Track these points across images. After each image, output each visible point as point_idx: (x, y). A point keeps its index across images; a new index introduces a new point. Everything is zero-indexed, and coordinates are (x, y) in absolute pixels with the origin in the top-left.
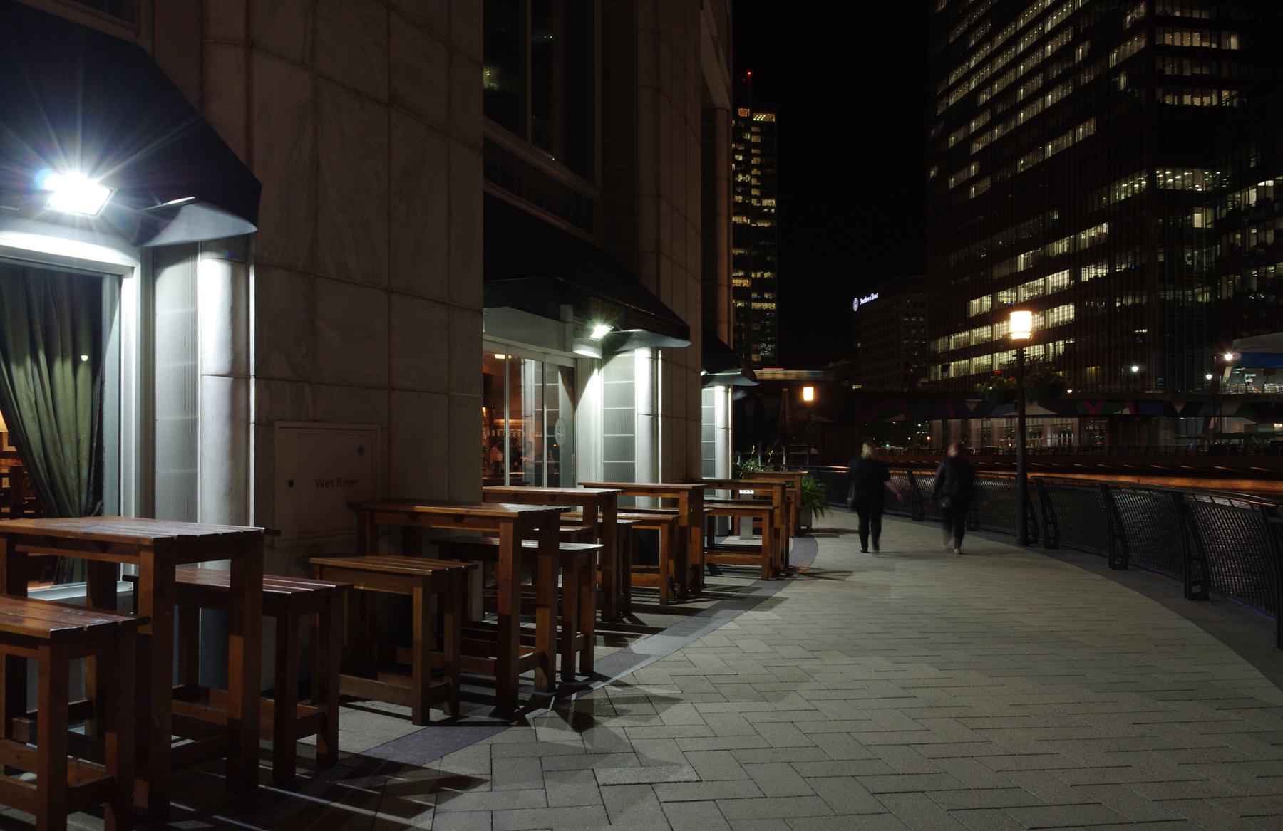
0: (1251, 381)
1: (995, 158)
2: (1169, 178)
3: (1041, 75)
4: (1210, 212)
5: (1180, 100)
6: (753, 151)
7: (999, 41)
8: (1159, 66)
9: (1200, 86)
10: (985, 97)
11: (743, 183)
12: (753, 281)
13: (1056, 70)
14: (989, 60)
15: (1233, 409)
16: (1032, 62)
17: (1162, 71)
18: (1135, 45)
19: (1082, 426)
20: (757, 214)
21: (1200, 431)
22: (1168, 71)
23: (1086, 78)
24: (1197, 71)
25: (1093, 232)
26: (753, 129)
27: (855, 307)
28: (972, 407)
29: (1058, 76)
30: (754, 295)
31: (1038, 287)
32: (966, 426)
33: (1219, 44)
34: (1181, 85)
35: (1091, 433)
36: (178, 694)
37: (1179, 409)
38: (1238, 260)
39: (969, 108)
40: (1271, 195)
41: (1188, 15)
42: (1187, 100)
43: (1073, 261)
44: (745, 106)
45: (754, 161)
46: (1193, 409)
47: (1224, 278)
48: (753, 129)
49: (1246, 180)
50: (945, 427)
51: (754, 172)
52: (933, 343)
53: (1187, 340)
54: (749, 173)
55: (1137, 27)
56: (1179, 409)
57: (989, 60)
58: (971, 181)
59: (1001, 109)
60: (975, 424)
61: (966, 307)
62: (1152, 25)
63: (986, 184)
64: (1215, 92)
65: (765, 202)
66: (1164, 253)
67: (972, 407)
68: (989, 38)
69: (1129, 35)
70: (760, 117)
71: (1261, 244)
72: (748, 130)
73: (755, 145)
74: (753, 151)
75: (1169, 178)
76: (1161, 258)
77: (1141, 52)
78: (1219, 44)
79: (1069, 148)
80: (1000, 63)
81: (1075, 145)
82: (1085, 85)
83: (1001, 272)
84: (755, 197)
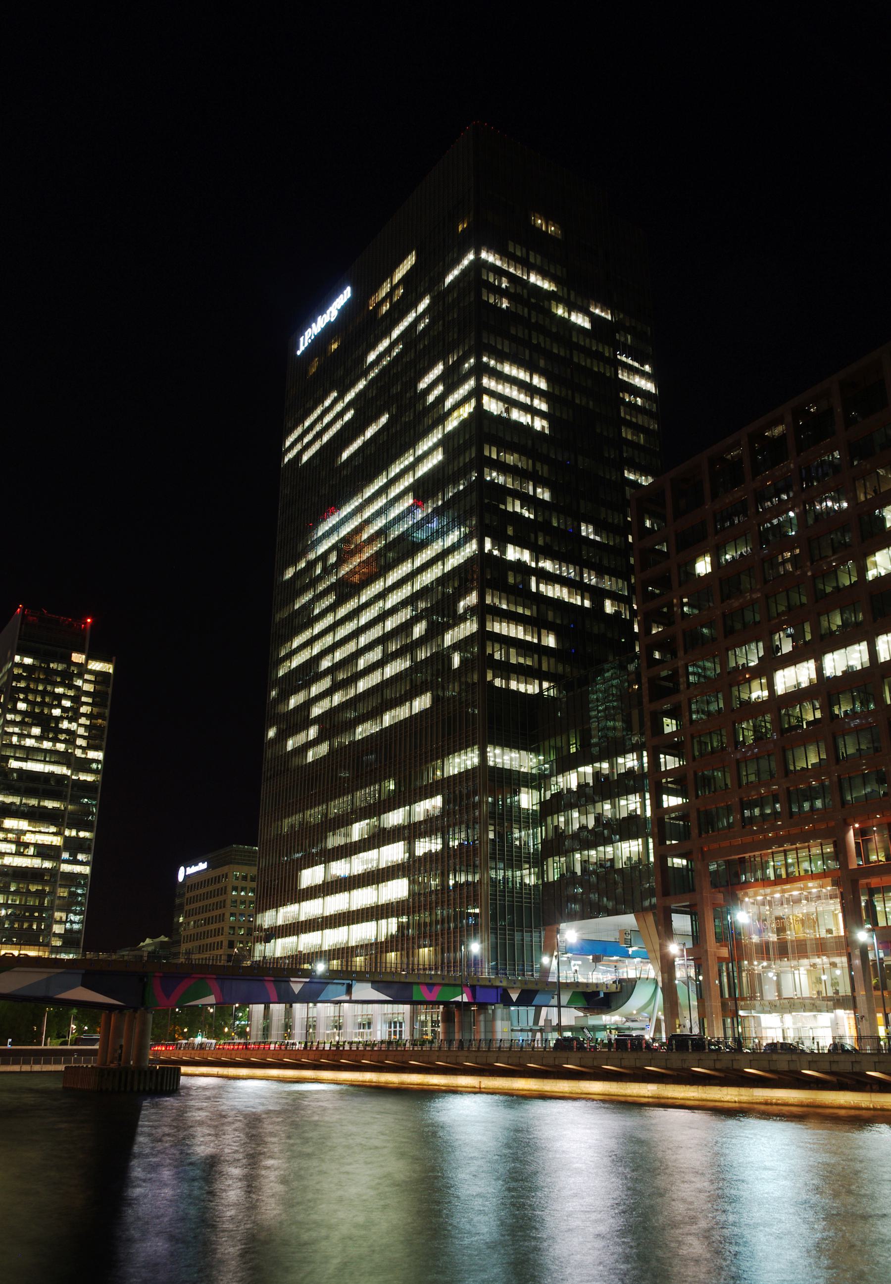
0: (577, 968)
1: (331, 724)
2: (502, 757)
3: (380, 647)
4: (536, 794)
5: (508, 684)
6: (84, 699)
7: (342, 612)
8: (489, 651)
9: (526, 673)
10: (326, 664)
11: (68, 731)
12: (67, 840)
13: (398, 642)
14: (332, 628)
15: (565, 998)
16: (376, 632)
17: (493, 655)
18: (469, 628)
19: (414, 1015)
20: (84, 765)
21: (531, 1023)
22: (497, 656)
23: (422, 654)
24: (521, 660)
25: (522, 688)
26: (87, 677)
27: (181, 878)
28: (297, 988)
29: (397, 650)
30: (65, 856)
31: (372, 860)
32: (289, 1014)
33: (539, 639)
34: (506, 670)
35: (424, 1024)
36: (609, 1049)
37: (514, 996)
38: (557, 844)
39: (308, 673)
40: (590, 781)
41: (513, 609)
42: (513, 685)
43: (409, 833)
44: (80, 651)
45: (84, 709)
46: (527, 998)
47: (550, 860)
48: (87, 677)
49: (565, 764)
50: (267, 1015)
51: (83, 720)
52: (259, 916)
53: (526, 917)
54: (76, 720)
55: (471, 611)
56: (514, 996)
57: (332, 628)
58: (309, 746)
59: (341, 676)
60: (299, 1009)
61: (296, 879)
62: (482, 612)
63: (323, 749)
64: (537, 682)
65: (92, 754)
66: (495, 831)
67: (297, 988)
68: (332, 608)
69: (463, 619)
70: (96, 666)
71: (583, 828)
72: (80, 676)
73: (87, 694)
74: (84, 699)
75: (502, 757)
76: (491, 836)
77: (472, 635)
78: (539, 639)
79: (406, 719)
80: (342, 632)
81: (411, 717)
82: (422, 661)
83: (334, 841)
84: (80, 747)
